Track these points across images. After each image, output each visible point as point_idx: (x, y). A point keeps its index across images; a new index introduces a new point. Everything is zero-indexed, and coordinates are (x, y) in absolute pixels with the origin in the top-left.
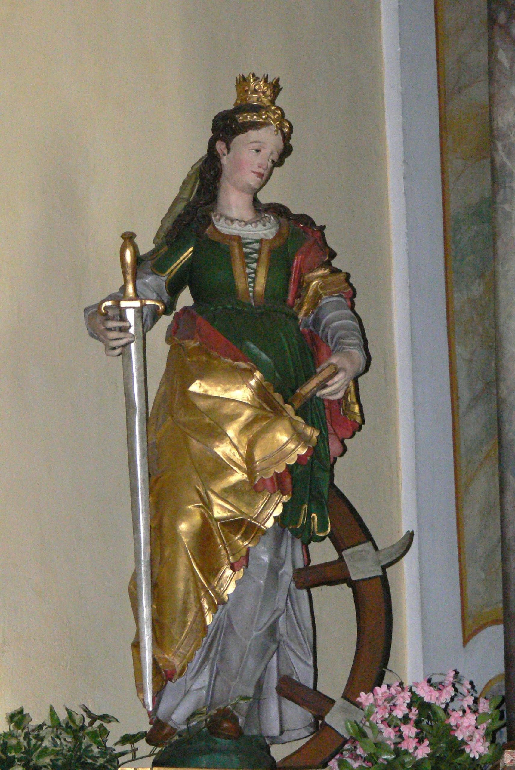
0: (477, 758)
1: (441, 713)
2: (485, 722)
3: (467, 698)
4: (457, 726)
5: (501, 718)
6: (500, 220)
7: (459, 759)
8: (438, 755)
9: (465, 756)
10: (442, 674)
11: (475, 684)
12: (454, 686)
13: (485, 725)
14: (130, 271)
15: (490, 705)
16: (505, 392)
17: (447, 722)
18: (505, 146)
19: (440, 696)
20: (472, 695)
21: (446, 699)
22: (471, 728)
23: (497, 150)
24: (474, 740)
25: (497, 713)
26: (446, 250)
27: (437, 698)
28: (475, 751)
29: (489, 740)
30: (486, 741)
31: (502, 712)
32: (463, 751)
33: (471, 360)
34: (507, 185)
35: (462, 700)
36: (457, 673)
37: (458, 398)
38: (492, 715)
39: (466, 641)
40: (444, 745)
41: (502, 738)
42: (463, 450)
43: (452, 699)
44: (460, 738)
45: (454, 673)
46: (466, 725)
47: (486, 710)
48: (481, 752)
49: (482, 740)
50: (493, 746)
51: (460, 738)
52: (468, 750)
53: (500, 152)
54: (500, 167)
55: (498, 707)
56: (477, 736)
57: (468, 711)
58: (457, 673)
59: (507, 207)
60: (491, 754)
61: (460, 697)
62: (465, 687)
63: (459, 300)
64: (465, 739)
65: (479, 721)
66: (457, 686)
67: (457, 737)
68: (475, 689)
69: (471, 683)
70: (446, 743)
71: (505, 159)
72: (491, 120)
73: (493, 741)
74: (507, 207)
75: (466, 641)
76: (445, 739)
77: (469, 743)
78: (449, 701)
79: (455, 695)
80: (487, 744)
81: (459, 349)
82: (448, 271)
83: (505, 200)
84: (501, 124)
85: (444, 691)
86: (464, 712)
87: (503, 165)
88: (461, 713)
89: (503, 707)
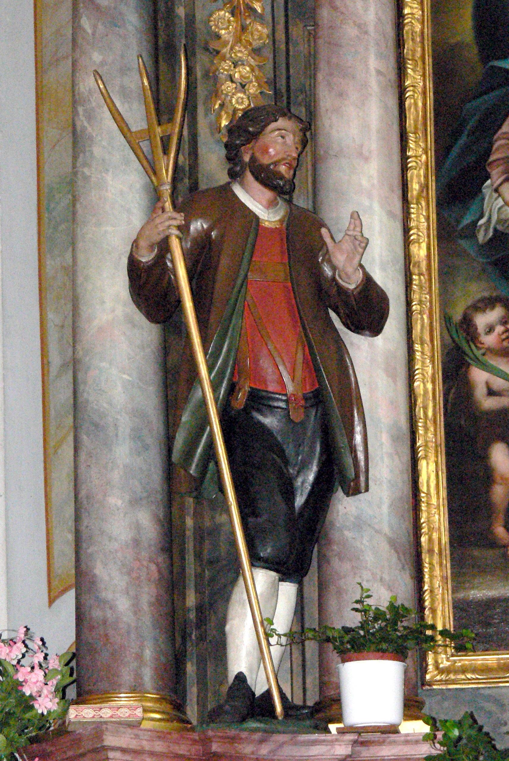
0: (45, 713)
1: (10, 670)
2: (55, 678)
3: (37, 655)
4: (26, 681)
5: (71, 675)
6: (80, 183)
7: (28, 715)
8: (7, 710)
9: (33, 713)
10: (13, 630)
11: (45, 640)
12: (24, 642)
13: (55, 682)
14: (355, 402)
15: (60, 662)
16: (81, 353)
17: (15, 677)
18: (85, 111)
19: (10, 652)
20: (42, 652)
21: (17, 656)
22: (38, 684)
23: (78, 114)
24: (42, 695)
25: (67, 669)
26: (39, 218)
27: (8, 654)
28: (43, 707)
29: (58, 696)
30: (56, 697)
31: (72, 669)
32: (32, 707)
33: (63, 326)
34: (87, 149)
35: (32, 656)
36: (28, 630)
37: (49, 363)
38: (61, 671)
39: (51, 601)
40: (13, 701)
41: (71, 692)
42: (53, 413)
43: (24, 656)
44: (28, 694)
45: (25, 629)
46: (34, 680)
47: (56, 667)
48: (49, 707)
49: (51, 696)
50: (63, 702)
51: (28, 694)
52: (36, 706)
53: (81, 117)
54: (81, 131)
55: (67, 664)
56: (45, 692)
57: (37, 668)
58: (28, 630)
59: (86, 171)
60: (60, 710)
61: (30, 653)
62: (36, 643)
63: (50, 264)
64: (34, 695)
65: (48, 677)
66: (27, 642)
67: (24, 693)
68: (46, 645)
69: (42, 640)
70: (16, 698)
71: (86, 124)
72: (74, 84)
73: (63, 697)
74: (86, 171)
75: (51, 601)
76: (14, 695)
77: (38, 698)
78: (20, 656)
79: (27, 651)
80: (57, 700)
81: (50, 315)
82: (42, 238)
83: (85, 164)
84: (82, 89)
85: (15, 647)
86: (33, 668)
87: (84, 129)
88: (29, 669)
89: (73, 664)
